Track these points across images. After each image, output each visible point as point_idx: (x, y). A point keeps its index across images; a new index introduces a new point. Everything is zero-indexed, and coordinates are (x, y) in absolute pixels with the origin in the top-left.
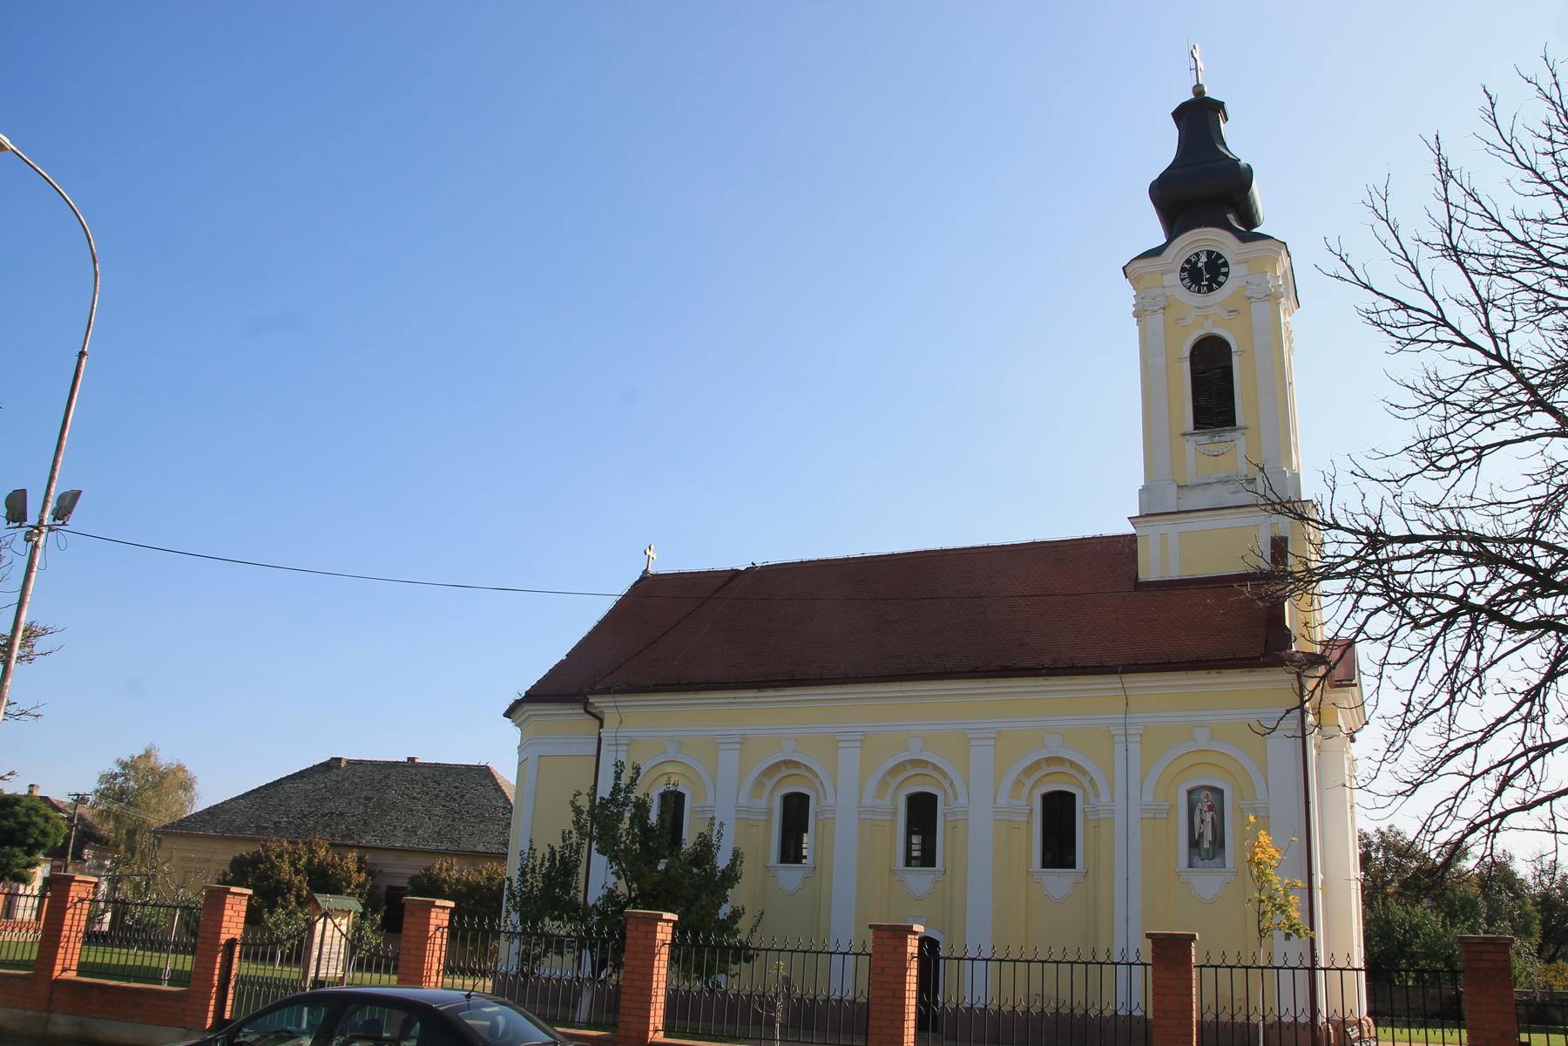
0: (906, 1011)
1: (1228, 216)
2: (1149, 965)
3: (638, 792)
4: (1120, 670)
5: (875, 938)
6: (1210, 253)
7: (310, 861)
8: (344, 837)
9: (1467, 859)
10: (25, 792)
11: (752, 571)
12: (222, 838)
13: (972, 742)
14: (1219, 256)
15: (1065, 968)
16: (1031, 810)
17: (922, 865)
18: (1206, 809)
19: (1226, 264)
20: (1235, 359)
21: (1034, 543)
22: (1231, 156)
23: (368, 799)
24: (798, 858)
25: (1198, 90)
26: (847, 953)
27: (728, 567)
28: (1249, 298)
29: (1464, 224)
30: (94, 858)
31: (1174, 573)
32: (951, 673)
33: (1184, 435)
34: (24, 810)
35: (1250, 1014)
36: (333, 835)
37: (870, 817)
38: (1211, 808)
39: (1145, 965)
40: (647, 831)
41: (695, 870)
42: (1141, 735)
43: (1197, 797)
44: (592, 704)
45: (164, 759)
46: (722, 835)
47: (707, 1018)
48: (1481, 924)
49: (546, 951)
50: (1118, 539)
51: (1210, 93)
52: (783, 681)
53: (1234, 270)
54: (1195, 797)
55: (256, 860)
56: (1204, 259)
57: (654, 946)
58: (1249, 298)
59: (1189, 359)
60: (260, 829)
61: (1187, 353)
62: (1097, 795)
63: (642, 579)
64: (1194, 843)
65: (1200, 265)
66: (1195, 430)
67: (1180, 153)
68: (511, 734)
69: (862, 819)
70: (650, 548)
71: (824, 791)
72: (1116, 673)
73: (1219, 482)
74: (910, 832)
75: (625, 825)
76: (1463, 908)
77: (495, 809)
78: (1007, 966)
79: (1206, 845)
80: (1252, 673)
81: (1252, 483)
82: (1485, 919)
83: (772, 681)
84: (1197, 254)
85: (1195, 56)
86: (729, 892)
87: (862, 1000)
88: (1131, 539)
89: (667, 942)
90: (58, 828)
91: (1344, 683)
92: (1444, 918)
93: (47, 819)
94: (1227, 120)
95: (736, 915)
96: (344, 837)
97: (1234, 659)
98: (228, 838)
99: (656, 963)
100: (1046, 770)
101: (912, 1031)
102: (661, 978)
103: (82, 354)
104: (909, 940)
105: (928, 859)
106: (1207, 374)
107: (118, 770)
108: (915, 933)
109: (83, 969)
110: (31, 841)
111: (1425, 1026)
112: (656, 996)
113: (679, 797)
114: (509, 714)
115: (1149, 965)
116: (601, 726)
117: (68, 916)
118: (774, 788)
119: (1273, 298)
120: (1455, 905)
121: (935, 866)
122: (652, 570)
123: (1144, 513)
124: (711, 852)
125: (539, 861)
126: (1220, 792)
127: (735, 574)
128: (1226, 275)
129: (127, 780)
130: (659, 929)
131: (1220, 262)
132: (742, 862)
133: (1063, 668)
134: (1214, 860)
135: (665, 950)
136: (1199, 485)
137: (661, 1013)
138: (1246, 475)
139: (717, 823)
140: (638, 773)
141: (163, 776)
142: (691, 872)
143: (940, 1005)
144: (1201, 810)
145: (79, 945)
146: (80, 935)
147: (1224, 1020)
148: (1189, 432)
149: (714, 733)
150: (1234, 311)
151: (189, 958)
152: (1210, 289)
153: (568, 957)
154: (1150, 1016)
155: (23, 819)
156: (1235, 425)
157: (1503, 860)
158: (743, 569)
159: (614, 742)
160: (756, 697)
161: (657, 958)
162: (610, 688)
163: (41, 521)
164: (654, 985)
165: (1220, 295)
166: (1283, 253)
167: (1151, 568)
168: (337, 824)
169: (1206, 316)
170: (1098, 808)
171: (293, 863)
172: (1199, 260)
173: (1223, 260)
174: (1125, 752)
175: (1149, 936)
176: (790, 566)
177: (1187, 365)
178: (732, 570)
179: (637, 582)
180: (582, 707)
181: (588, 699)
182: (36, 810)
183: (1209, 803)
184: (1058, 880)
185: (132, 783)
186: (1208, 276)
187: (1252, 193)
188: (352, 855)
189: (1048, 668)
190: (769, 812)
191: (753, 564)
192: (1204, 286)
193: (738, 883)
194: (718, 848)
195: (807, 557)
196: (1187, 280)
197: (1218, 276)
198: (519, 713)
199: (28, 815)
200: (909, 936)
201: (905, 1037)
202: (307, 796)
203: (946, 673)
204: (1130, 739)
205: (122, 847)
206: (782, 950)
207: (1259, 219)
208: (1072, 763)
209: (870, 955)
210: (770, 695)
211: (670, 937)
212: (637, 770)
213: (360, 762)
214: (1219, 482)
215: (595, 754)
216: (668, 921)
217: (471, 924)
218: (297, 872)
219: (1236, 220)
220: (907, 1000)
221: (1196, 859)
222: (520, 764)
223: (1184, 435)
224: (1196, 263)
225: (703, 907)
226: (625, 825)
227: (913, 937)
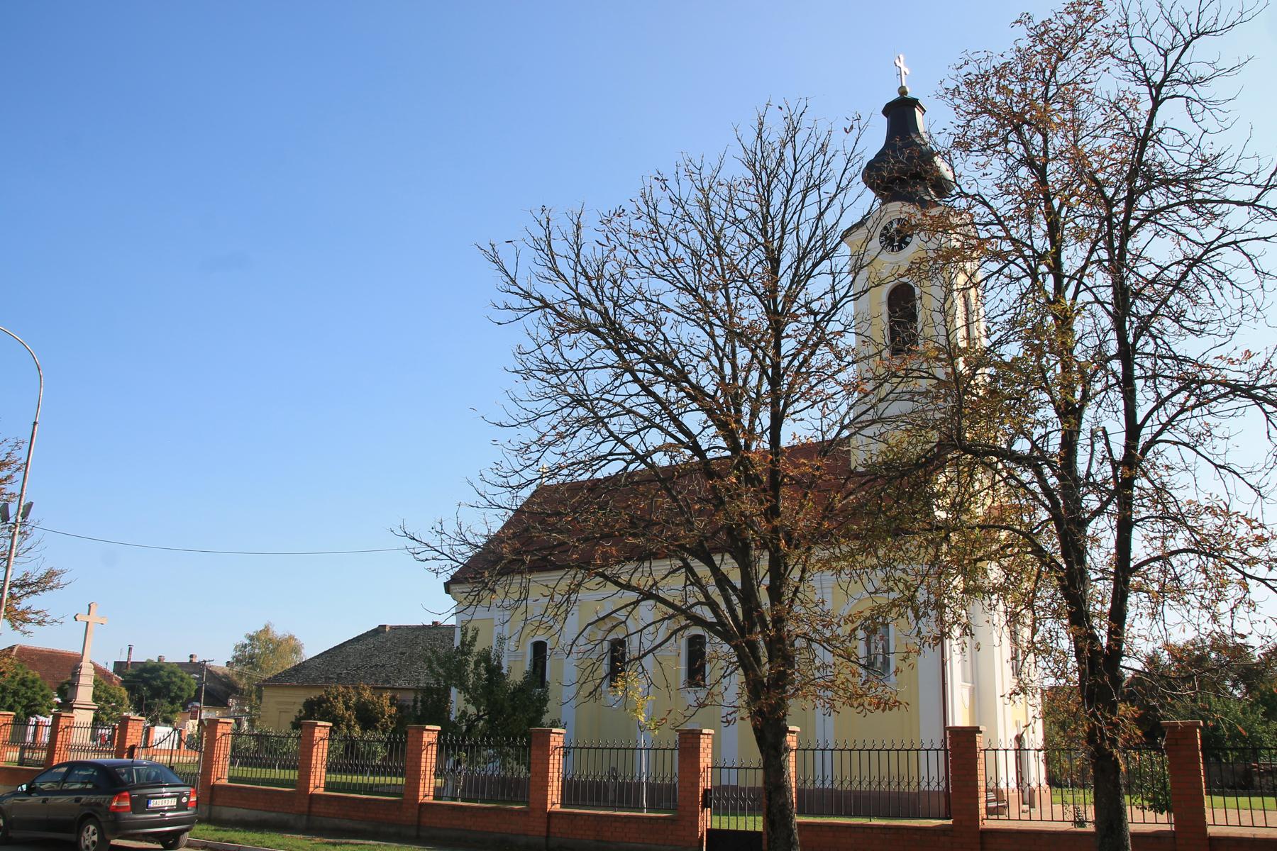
8: (384, 682)
10: (188, 660)
12: (302, 687)
23: (402, 653)
25: (903, 91)
29: (540, 348)
30: (237, 704)
34: (166, 674)
36: (376, 681)
45: (279, 631)
47: (476, 792)
51: (911, 94)
55: (320, 701)
60: (328, 679)
79: (879, 665)
90: (190, 685)
93: (182, 679)
96: (384, 682)
98: (307, 687)
99: (551, 761)
103: (35, 423)
107: (247, 642)
109: (328, 786)
110: (172, 694)
111: (1223, 794)
129: (254, 648)
130: (551, 739)
140: (477, 634)
141: (279, 644)
145: (323, 774)
152: (900, 248)
155: (166, 680)
161: (552, 757)
163: (16, 520)
168: (380, 673)
171: (345, 703)
182: (174, 673)
185: (257, 651)
188: (388, 694)
199: (169, 677)
202: (361, 654)
204: (825, 591)
205: (254, 696)
212: (476, 631)
213: (400, 627)
217: (401, 739)
218: (348, 708)
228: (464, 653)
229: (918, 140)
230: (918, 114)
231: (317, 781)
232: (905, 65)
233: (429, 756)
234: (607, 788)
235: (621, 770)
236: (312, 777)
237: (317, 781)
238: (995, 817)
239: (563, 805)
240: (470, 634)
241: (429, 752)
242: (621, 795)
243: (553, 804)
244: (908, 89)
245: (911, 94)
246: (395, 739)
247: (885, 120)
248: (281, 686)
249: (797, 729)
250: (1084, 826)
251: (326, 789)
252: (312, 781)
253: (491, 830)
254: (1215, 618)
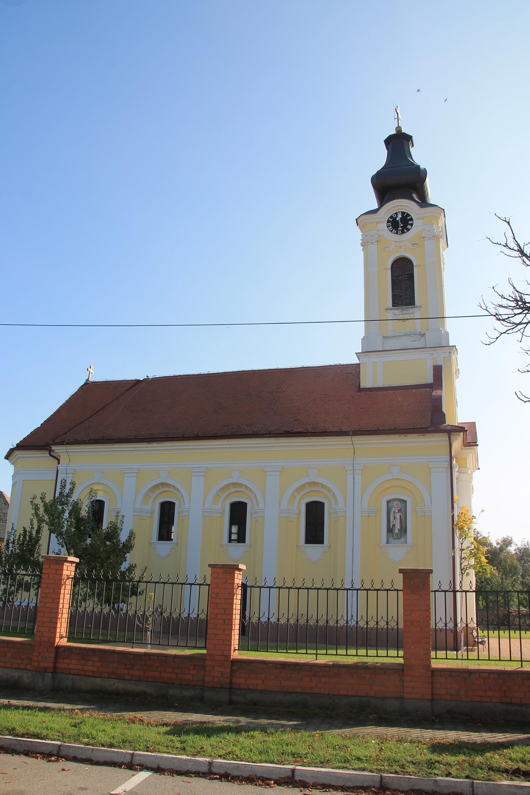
0: (233, 623)
1: (413, 195)
2: (400, 590)
3: (74, 497)
4: (351, 433)
5: (213, 573)
6: (403, 213)
9: (511, 546)
11: (147, 381)
13: (267, 473)
14: (408, 215)
16: (300, 511)
17: (238, 542)
18: (397, 511)
19: (411, 219)
21: (303, 368)
22: (415, 164)
24: (169, 539)
25: (398, 129)
26: (193, 584)
27: (133, 378)
28: (424, 238)
31: (380, 384)
32: (256, 434)
33: (387, 309)
35: (358, 621)
37: (209, 514)
38: (399, 511)
39: (397, 590)
40: (79, 521)
41: (108, 543)
42: (362, 470)
43: (392, 505)
44: (54, 451)
46: (123, 522)
48: (519, 578)
49: (18, 590)
50: (349, 366)
52: (161, 438)
53: (415, 222)
54: (391, 504)
56: (400, 216)
57: (61, 580)
58: (424, 238)
59: (390, 269)
61: (389, 266)
62: (337, 503)
63: (86, 384)
64: (390, 530)
65: (398, 219)
66: (393, 307)
67: (389, 159)
68: (9, 468)
69: (205, 516)
70: (90, 367)
71: (184, 501)
72: (349, 435)
73: (405, 335)
74: (231, 524)
75: (66, 515)
76: (510, 570)
77: (4, 514)
78: (303, 592)
79: (396, 531)
80: (425, 436)
81: (423, 336)
82: (521, 576)
83: (155, 438)
84: (396, 214)
85: (397, 112)
86: (127, 555)
87: (203, 616)
88: (357, 366)
89: (71, 577)
91: (471, 444)
92: (502, 575)
94: (413, 146)
95: (131, 569)
97: (414, 428)
99: (62, 591)
100: (308, 489)
101: (237, 637)
102: (66, 601)
104: (236, 575)
105: (241, 539)
106: (400, 278)
108: (240, 570)
112: (62, 613)
113: (101, 503)
114: (7, 457)
115: (400, 590)
116: (59, 463)
118: (155, 498)
119: (436, 238)
120: (506, 568)
121: (245, 543)
122: (91, 379)
123: (364, 351)
124: (117, 532)
125: (17, 537)
126: (405, 502)
127: (138, 382)
128: (412, 225)
130: (65, 567)
131: (408, 218)
132: (134, 538)
133: (319, 432)
134: (400, 540)
135: (69, 582)
136: (395, 337)
137: (64, 625)
138: (420, 332)
139: (121, 514)
140: (74, 487)
142: (105, 544)
143: (247, 618)
144: (394, 512)
147: (202, 618)
148: (390, 308)
149: (122, 467)
150: (416, 244)
152: (403, 232)
153: (33, 592)
154: (401, 626)
156: (415, 305)
157: (527, 547)
158: (141, 379)
159: (65, 472)
160: (146, 447)
162: (64, 441)
164: (61, 606)
165: (408, 235)
166: (442, 214)
167: (366, 382)
169: (400, 247)
170: (337, 510)
172: (397, 216)
173: (410, 217)
174: (353, 479)
175: (401, 571)
176: (168, 378)
177: (389, 273)
178: (135, 380)
179: (82, 386)
180: (48, 452)
181: (51, 448)
183: (399, 508)
184: (314, 549)
186: (402, 225)
187: (426, 183)
189: (311, 432)
190: (152, 512)
191: (147, 377)
192: (399, 230)
193: (132, 550)
194: (121, 530)
195: (177, 373)
196: (391, 227)
197: (407, 226)
198: (12, 456)
200: (236, 572)
201: (233, 641)
203: (254, 434)
204: (355, 472)
206: (149, 582)
207: (429, 199)
208: (323, 486)
209: (209, 585)
210: (154, 446)
211: (73, 574)
212: (73, 484)
214: (405, 335)
215: (55, 479)
216: (72, 562)
219: (417, 198)
220: (234, 616)
221: (391, 539)
222: (13, 485)
223: (387, 309)
224: (396, 218)
225: (111, 563)
226: (66, 515)
227: (239, 572)
228: (62, 504)
238: (304, 651)
240: (68, 486)
250: (464, 646)
254: (485, 757)
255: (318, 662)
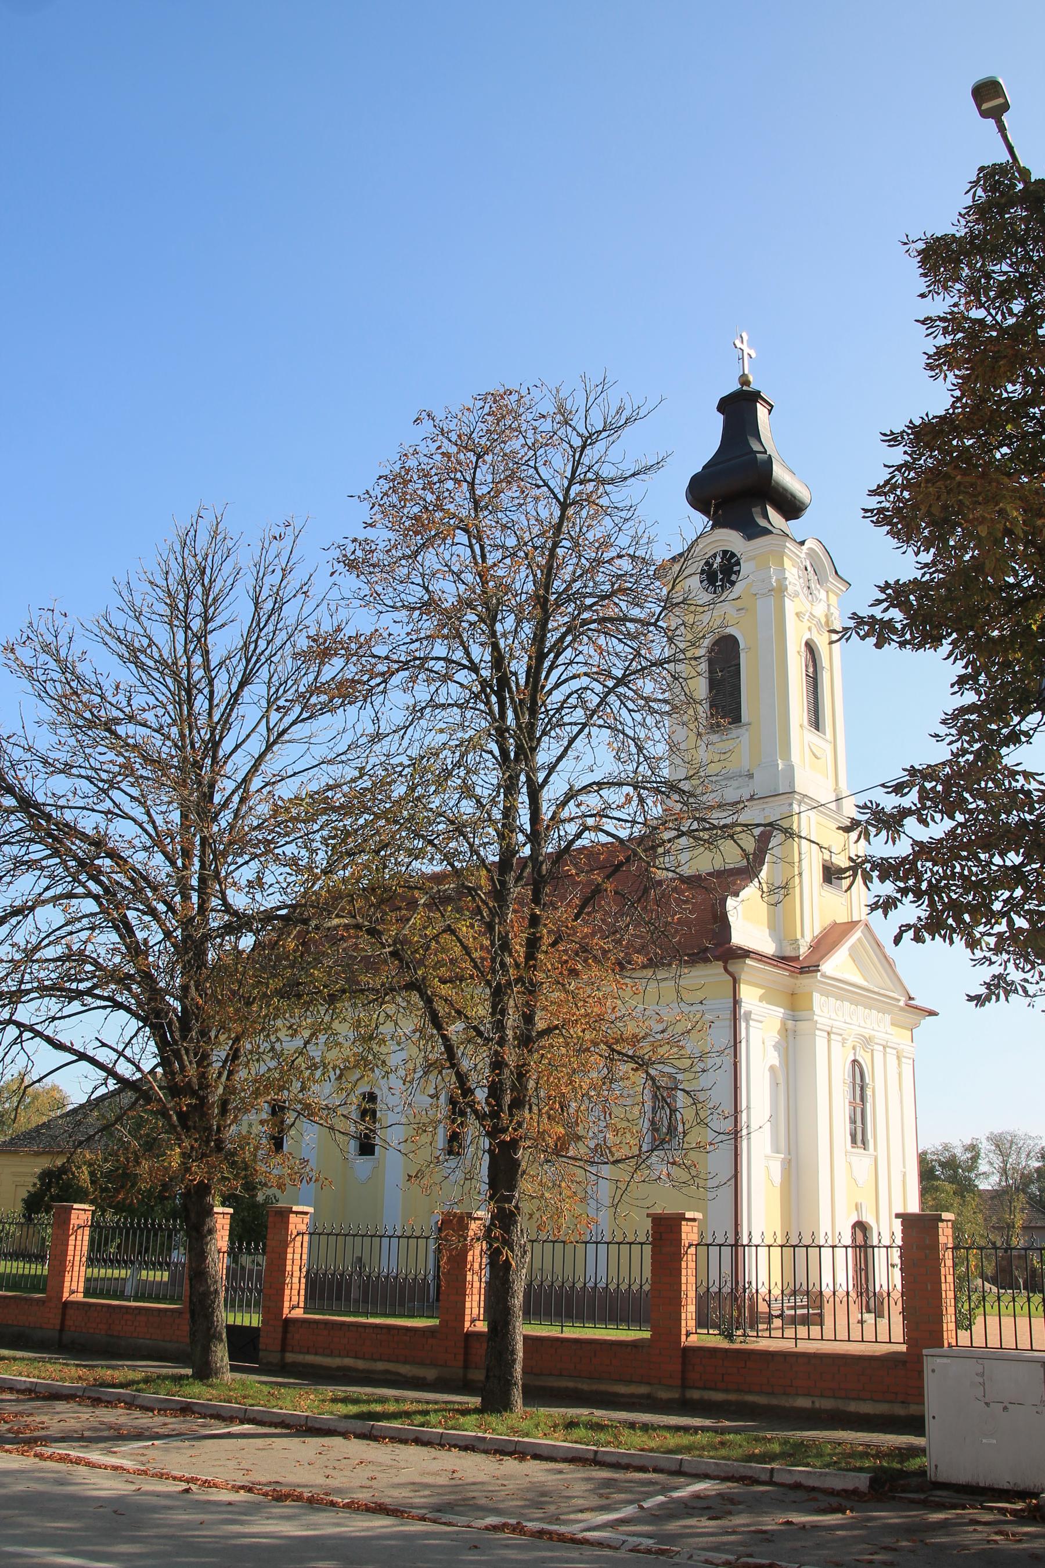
6: (725, 552)
7: (102, 1173)
14: (733, 555)
15: (394, 1240)
20: (742, 655)
25: (744, 381)
53: (745, 568)
65: (715, 566)
104: (940, 1230)
109: (92, 1288)
117: (71, 1242)
146: (84, 1259)
151: (167, 1273)
161: (73, 1237)
196: (706, 582)
217: (139, 1224)
229: (756, 447)
230: (761, 411)
231: (74, 1284)
232: (750, 346)
233: (79, 1243)
234: (349, 1285)
235: (366, 1259)
236: (67, 1278)
237: (295, 1298)
239: (306, 1310)
241: (79, 1238)
242: (366, 1293)
243: (72, 1292)
244: (751, 378)
245: (754, 386)
246: (132, 1224)
247: (718, 421)
248: (16, 1152)
249: (698, 1215)
251: (87, 1293)
252: (67, 1284)
253: (10, 1322)
255: (563, 1335)
